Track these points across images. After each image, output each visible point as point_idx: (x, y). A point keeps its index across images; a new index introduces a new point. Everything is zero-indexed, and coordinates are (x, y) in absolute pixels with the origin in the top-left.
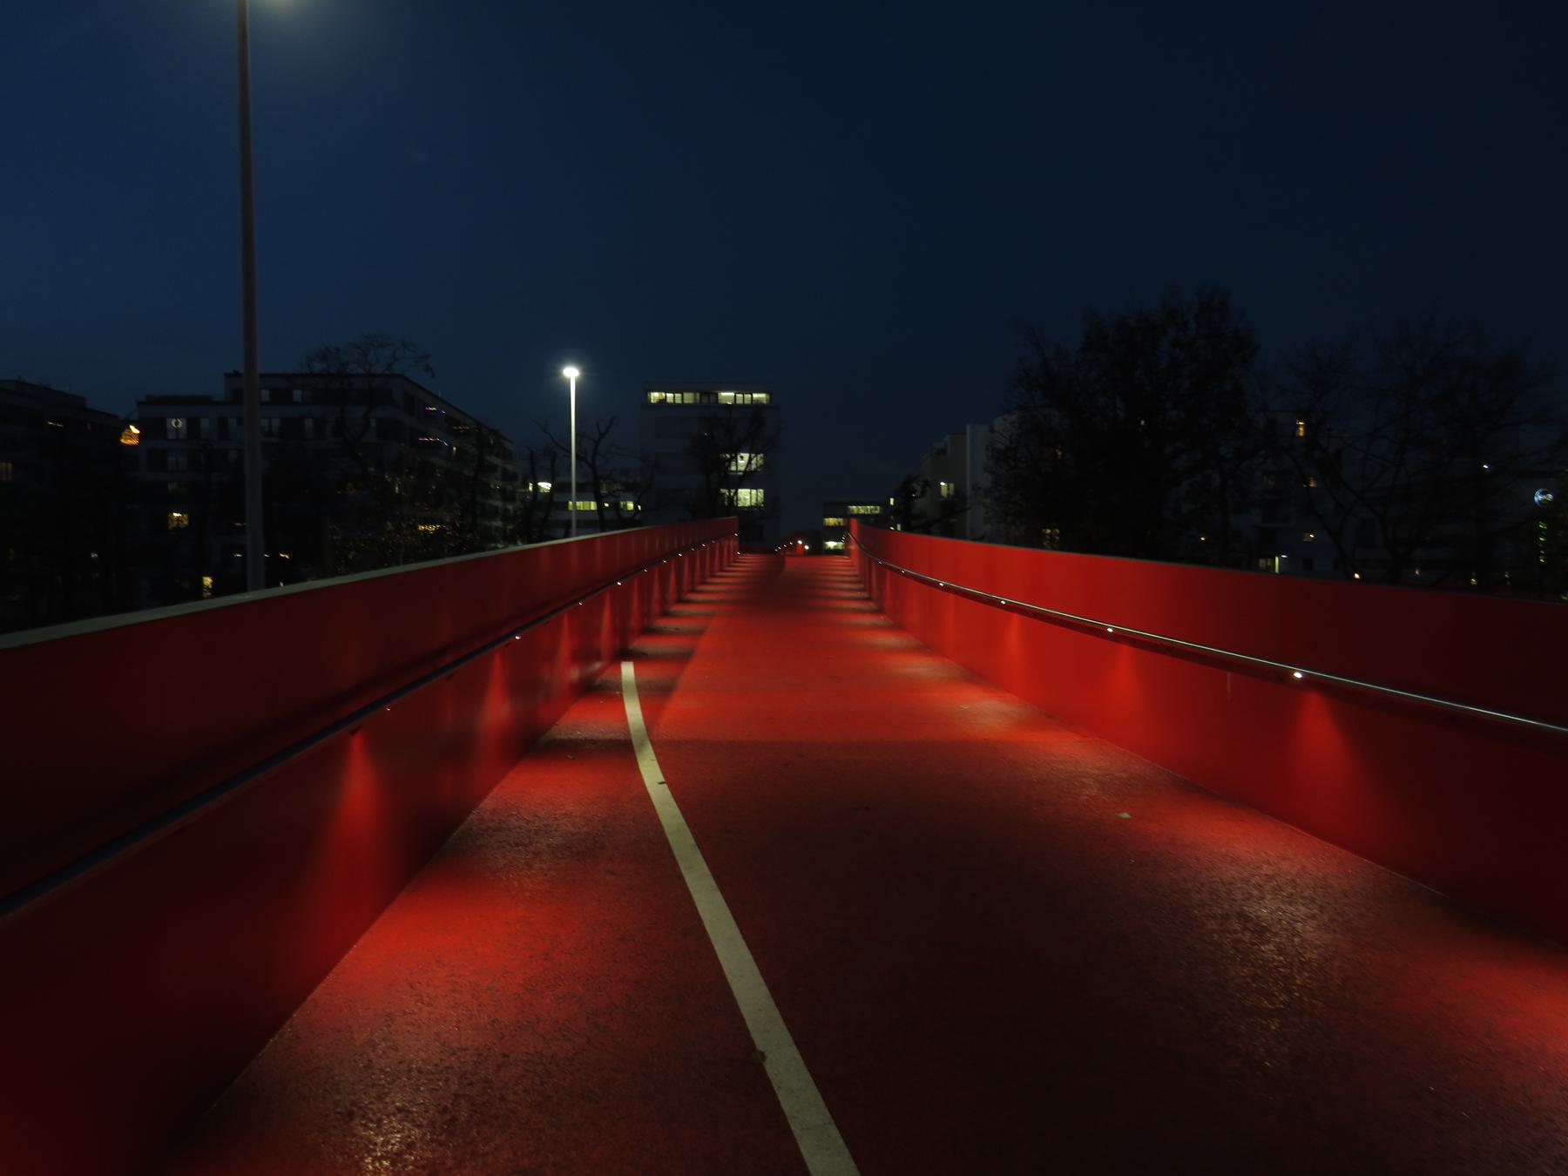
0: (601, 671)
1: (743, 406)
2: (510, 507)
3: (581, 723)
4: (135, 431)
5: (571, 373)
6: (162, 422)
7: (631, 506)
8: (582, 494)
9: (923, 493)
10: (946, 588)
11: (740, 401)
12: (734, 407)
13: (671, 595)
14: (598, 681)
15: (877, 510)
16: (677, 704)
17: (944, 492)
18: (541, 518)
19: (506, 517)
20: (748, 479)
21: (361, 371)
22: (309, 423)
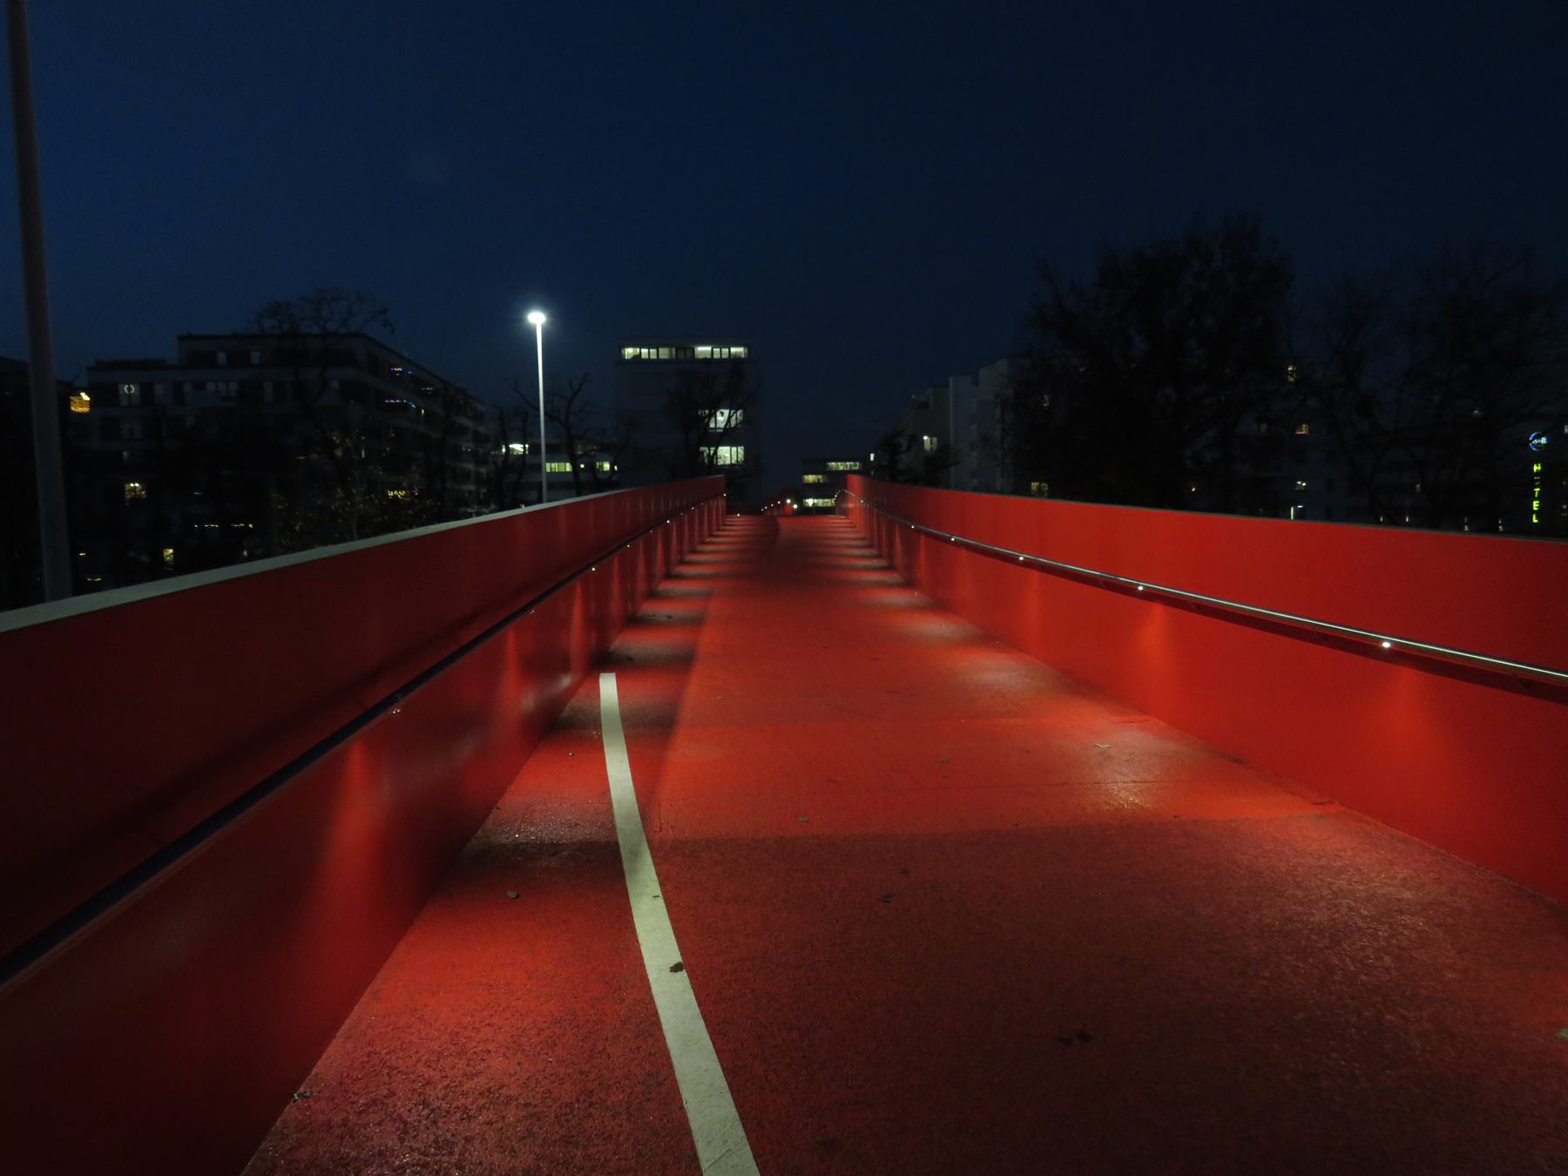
0: (572, 691)
1: (721, 360)
2: (483, 470)
3: (536, 805)
4: (85, 397)
5: (537, 319)
6: (113, 390)
7: (607, 466)
8: (554, 453)
9: (909, 449)
10: (1026, 564)
11: (716, 356)
12: (709, 362)
13: (659, 569)
14: (567, 711)
15: (857, 466)
16: (686, 752)
17: (927, 446)
18: (513, 483)
19: (479, 481)
20: (728, 436)
21: (316, 330)
22: (268, 387)
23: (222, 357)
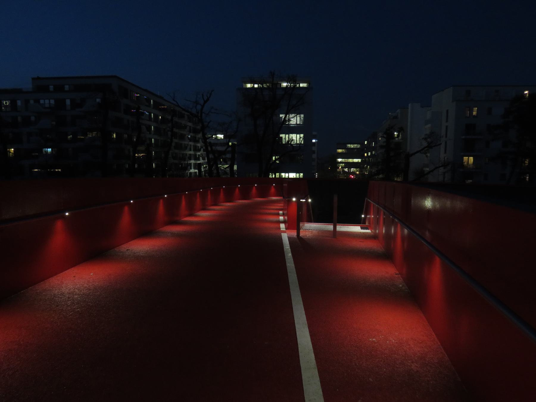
5: (284, 85)
20: (368, 154)
22: (68, 102)
23: (51, 88)
